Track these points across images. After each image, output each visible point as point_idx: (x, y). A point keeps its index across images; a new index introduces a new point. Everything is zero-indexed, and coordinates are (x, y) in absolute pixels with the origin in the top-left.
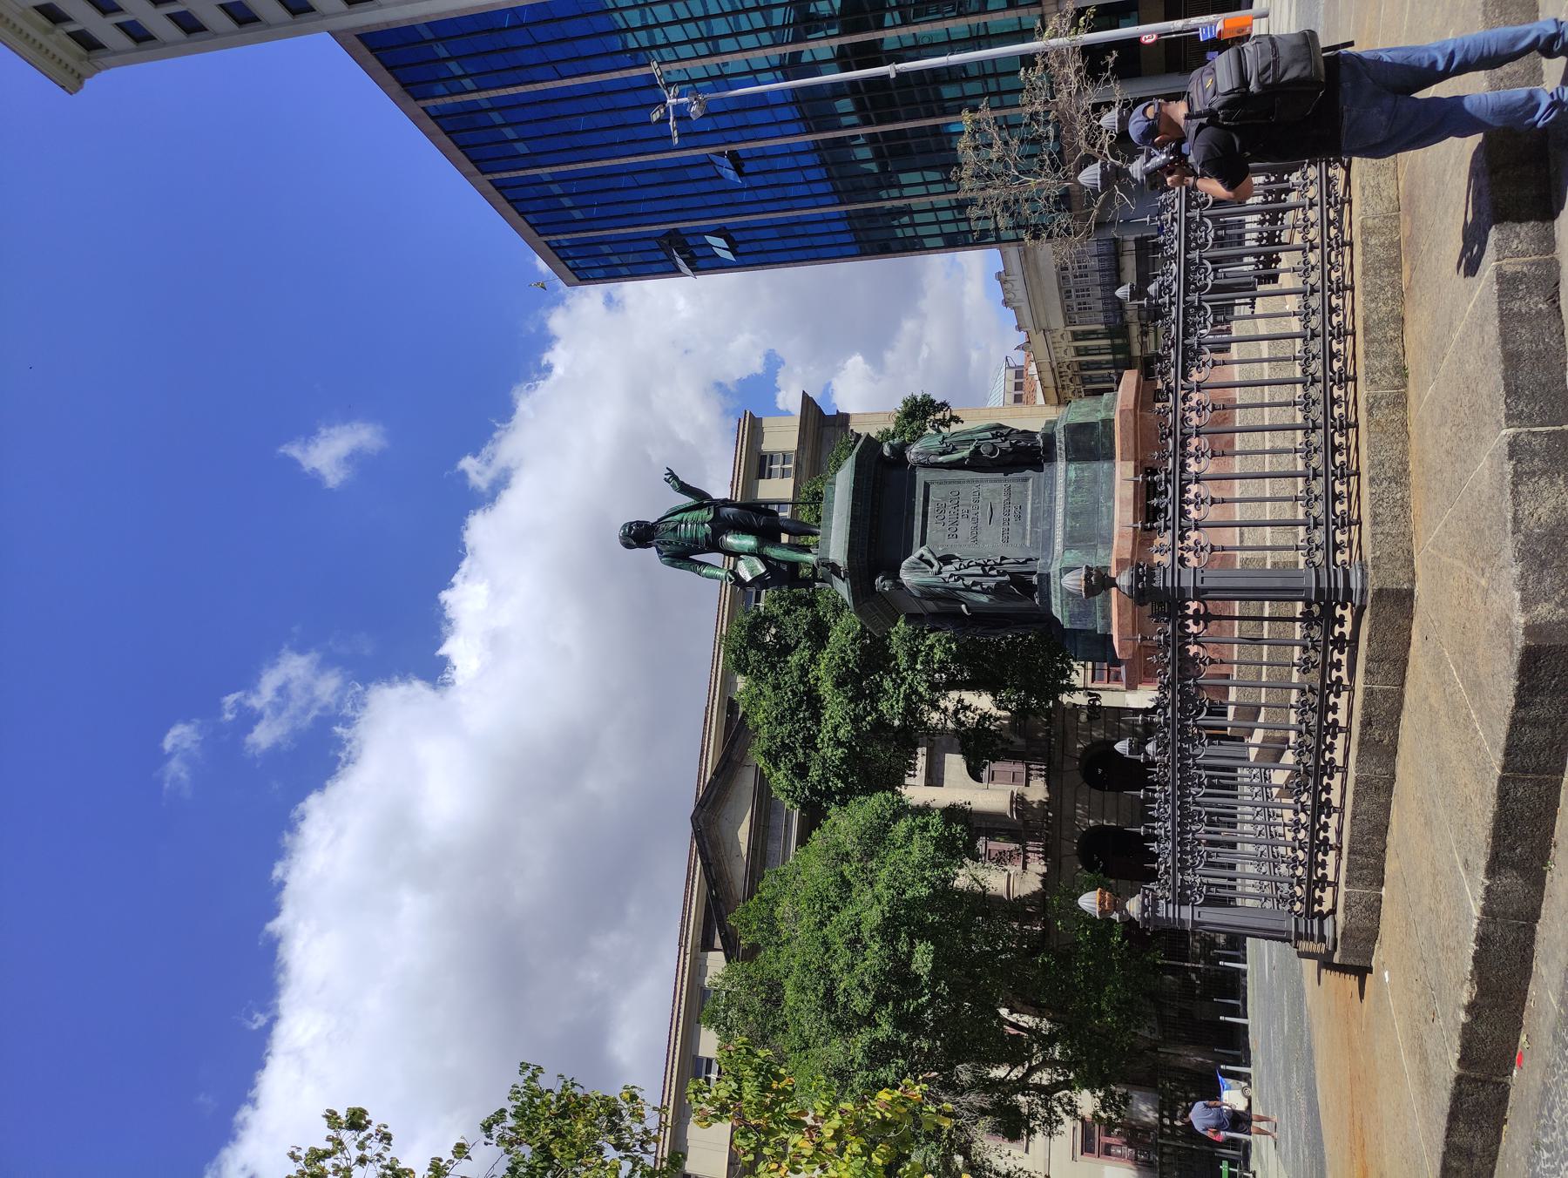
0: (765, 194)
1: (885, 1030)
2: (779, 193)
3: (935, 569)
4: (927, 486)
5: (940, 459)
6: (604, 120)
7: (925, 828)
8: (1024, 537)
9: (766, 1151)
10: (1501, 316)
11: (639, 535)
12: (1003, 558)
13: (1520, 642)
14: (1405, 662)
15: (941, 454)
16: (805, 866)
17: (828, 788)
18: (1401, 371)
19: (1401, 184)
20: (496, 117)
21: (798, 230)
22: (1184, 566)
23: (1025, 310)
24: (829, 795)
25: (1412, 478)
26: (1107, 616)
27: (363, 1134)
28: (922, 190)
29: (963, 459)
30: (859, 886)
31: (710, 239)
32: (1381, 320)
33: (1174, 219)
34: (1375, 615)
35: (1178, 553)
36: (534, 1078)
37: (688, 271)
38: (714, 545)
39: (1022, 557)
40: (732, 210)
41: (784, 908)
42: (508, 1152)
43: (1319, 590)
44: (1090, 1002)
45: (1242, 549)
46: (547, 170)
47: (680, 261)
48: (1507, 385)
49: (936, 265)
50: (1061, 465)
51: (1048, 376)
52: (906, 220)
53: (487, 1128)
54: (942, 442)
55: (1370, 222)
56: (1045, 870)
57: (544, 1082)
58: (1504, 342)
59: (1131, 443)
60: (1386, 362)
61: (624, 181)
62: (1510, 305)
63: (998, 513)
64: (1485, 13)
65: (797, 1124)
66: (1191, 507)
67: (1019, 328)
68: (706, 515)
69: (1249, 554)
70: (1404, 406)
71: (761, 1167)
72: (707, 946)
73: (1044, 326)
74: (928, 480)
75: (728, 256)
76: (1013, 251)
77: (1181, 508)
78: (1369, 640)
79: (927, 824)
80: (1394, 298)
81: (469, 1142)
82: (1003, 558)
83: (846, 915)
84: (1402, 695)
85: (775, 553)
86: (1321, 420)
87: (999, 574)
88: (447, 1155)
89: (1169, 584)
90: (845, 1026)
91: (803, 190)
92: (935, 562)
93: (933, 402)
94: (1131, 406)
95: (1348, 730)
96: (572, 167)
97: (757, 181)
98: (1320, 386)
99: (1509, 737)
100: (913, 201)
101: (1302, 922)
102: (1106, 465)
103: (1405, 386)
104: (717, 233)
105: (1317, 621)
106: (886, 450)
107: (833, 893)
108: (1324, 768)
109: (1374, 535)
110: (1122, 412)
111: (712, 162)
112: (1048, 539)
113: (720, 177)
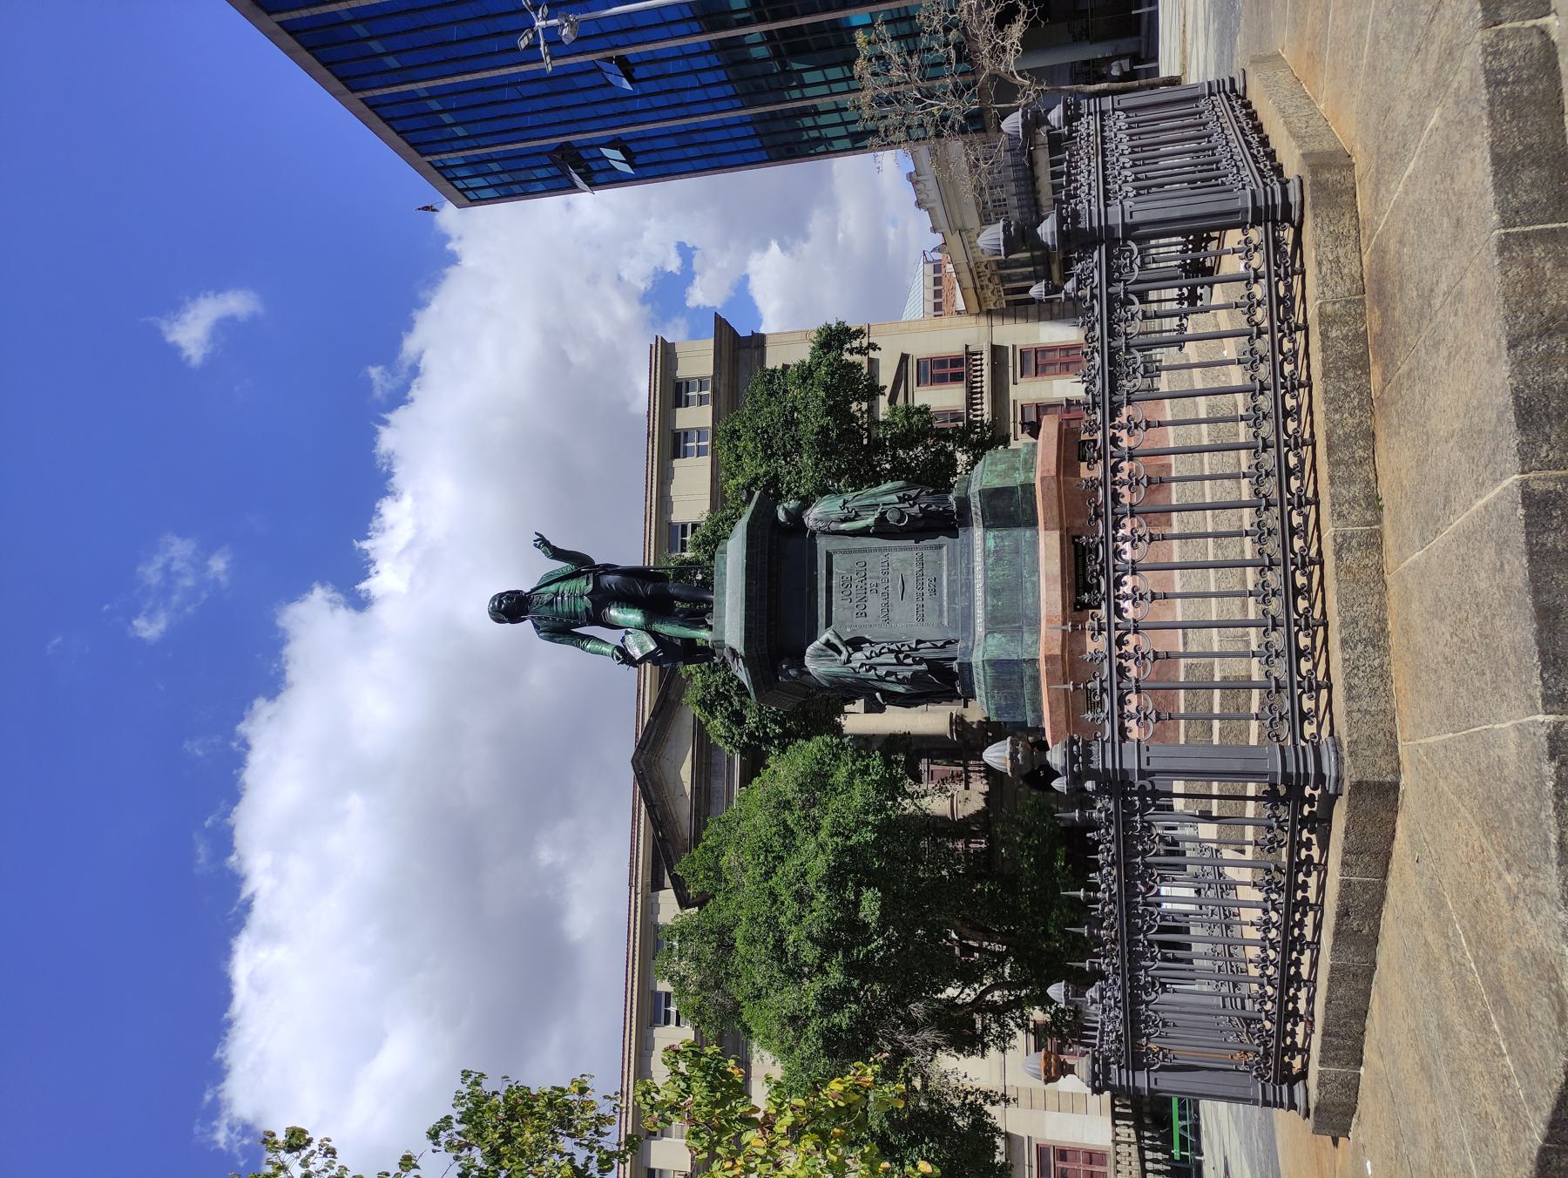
0: (658, 101)
1: (836, 977)
2: (674, 98)
3: (844, 657)
4: (829, 556)
5: (843, 526)
6: (480, 28)
7: (865, 771)
8: (941, 614)
9: (719, 1150)
11: (510, 608)
12: (919, 642)
14: (1388, 855)
17: (765, 733)
18: (1374, 502)
19: (1365, 259)
20: (360, 30)
21: (698, 138)
22: (1116, 446)
23: (940, 211)
24: (768, 740)
25: (1393, 641)
26: (1037, 710)
27: (304, 1153)
28: (824, 90)
29: (868, 527)
30: (802, 834)
31: (606, 152)
32: (1348, 436)
35: (1110, 432)
37: (585, 187)
38: (597, 618)
40: (626, 119)
41: (729, 858)
42: (457, 1158)
43: (1286, 777)
44: (1037, 927)
45: (1186, 655)
46: (422, 85)
47: (576, 177)
48: (1542, 653)
49: (845, 168)
50: (978, 532)
51: (966, 277)
52: (808, 122)
53: (434, 1135)
55: (1329, 308)
56: (987, 788)
57: (487, 1087)
58: (1536, 592)
59: (1056, 512)
60: (1356, 489)
61: (507, 93)
62: (1542, 538)
64: (1491, 115)
65: (747, 1121)
66: (1130, 663)
67: (934, 230)
68: (584, 585)
70: (1379, 547)
71: (716, 1166)
72: (657, 885)
73: (959, 225)
74: (830, 549)
75: (626, 168)
76: (923, 150)
77: (1122, 726)
79: (867, 766)
80: (1361, 407)
81: (415, 1153)
82: (919, 642)
83: (792, 863)
84: (1384, 887)
85: (667, 629)
86: (1279, 556)
87: (916, 662)
89: (1124, 1082)
90: (795, 975)
91: (699, 95)
93: (848, 329)
94: (1053, 473)
96: (449, 81)
97: (650, 87)
98: (1276, 511)
99: (1555, 1112)
100: (817, 101)
101: (1270, 1088)
102: (1028, 533)
103: (1379, 521)
104: (614, 144)
105: (1284, 801)
106: (782, 516)
107: (777, 843)
108: (1293, 942)
109: (1349, 713)
110: (1042, 479)
111: (599, 69)
113: (609, 84)
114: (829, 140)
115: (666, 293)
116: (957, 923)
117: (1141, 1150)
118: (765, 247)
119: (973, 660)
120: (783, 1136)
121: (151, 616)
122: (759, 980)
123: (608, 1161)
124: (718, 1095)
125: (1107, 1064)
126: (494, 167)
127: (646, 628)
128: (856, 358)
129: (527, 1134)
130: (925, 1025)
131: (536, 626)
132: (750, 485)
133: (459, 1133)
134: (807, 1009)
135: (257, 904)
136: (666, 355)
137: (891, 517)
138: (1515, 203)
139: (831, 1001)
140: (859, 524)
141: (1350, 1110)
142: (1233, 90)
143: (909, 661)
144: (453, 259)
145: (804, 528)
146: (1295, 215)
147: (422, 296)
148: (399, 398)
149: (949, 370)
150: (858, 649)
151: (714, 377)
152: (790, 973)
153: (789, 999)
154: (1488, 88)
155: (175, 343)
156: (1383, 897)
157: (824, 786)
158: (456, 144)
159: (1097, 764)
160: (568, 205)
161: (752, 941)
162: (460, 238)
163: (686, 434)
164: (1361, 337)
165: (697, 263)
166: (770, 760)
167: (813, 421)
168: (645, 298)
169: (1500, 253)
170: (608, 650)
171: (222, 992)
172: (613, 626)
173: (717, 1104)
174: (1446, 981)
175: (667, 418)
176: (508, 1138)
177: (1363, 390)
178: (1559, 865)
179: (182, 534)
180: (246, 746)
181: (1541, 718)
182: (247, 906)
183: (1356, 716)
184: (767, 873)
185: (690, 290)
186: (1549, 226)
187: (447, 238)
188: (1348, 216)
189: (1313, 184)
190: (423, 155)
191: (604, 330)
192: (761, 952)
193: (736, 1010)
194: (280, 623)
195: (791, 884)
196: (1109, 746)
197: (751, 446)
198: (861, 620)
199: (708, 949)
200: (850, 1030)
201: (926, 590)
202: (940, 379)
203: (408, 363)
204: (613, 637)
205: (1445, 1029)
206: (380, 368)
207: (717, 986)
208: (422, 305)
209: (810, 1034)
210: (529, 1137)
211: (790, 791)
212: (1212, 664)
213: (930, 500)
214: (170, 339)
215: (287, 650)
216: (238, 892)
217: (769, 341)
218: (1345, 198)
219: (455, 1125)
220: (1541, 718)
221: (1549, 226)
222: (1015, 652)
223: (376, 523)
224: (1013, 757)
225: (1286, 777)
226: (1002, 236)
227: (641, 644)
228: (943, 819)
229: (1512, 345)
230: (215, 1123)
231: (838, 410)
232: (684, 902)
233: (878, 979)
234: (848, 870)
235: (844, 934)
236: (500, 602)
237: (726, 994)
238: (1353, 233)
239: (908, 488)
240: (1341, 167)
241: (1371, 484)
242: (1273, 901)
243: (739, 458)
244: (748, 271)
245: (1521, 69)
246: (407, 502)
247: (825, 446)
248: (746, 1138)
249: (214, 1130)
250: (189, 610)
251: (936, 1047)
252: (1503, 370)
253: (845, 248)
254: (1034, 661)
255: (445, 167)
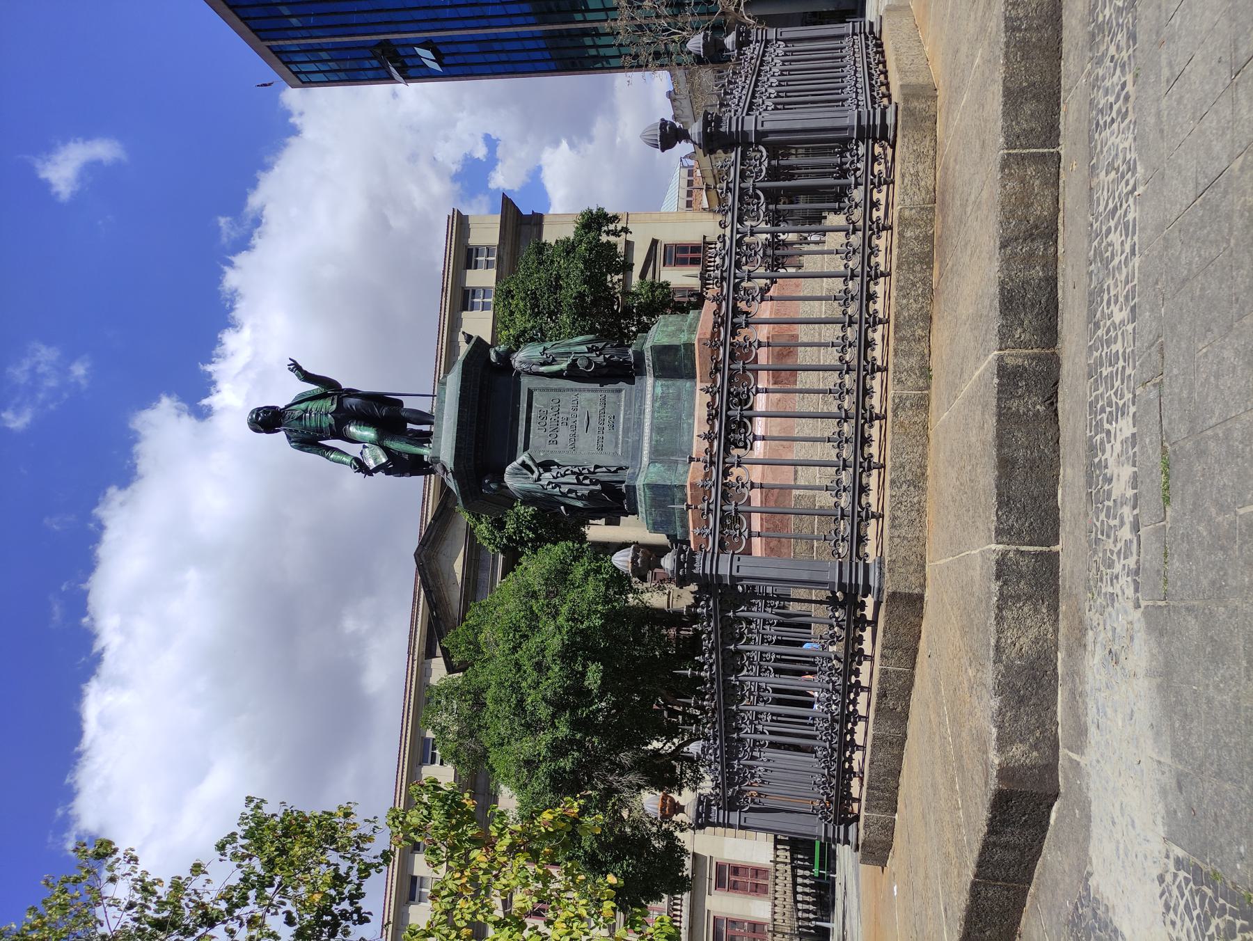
1: (563, 731)
4: (530, 393)
5: (542, 369)
7: (598, 571)
8: (616, 446)
10: (999, 415)
12: (596, 467)
13: (993, 784)
14: (916, 651)
15: (543, 364)
16: (505, 594)
17: (521, 538)
21: (497, 46)
24: (523, 543)
29: (562, 371)
30: (544, 618)
31: (420, 51)
33: (728, 189)
34: (889, 613)
36: (258, 807)
39: (613, 463)
42: (239, 866)
47: (393, 69)
48: (999, 495)
50: (650, 380)
52: (588, 41)
53: (221, 847)
54: (543, 353)
55: (907, 213)
57: (267, 810)
58: (1000, 446)
60: (914, 361)
63: (594, 421)
64: (1006, 56)
68: (329, 405)
69: (801, 492)
70: (927, 409)
72: (430, 654)
74: (532, 387)
75: (435, 66)
78: (885, 632)
81: (204, 861)
82: (596, 467)
84: (913, 676)
85: (396, 446)
87: (592, 483)
88: (185, 874)
90: (532, 727)
92: (535, 469)
93: (606, 215)
95: (869, 689)
98: (854, 375)
99: (981, 855)
101: (830, 827)
102: (688, 384)
103: (928, 388)
104: (426, 44)
105: (842, 605)
106: (493, 357)
109: (891, 538)
110: (699, 340)
112: (637, 448)
114: (607, 58)
115: (472, 175)
116: (664, 692)
117: (794, 869)
118: (557, 143)
119: (637, 483)
120: (504, 853)
121: (18, 412)
122: (502, 730)
123: (366, 870)
124: (454, 821)
125: (709, 806)
126: (324, 55)
127: (379, 443)
128: (612, 239)
129: (297, 848)
130: (631, 769)
131: (288, 438)
132: (519, 336)
133: (242, 846)
134: (539, 754)
135: (107, 656)
136: (460, 224)
137: (581, 364)
138: (1017, 129)
139: (558, 749)
140: (555, 368)
141: (888, 846)
142: (871, 32)
143: (587, 482)
144: (295, 131)
145: (511, 368)
146: (891, 135)
147: (267, 160)
148: (244, 244)
149: (690, 255)
150: (547, 470)
151: (499, 246)
152: (528, 726)
153: (526, 747)
154: (1006, 32)
155: (47, 179)
156: (912, 684)
157: (566, 580)
158: (290, 33)
159: (698, 570)
160: (395, 95)
161: (498, 701)
162: (301, 114)
163: (474, 291)
164: (929, 239)
165: (500, 152)
166: (523, 559)
167: (574, 286)
168: (456, 178)
169: (1002, 169)
170: (348, 460)
171: (71, 729)
172: (352, 441)
173: (454, 828)
174: (937, 752)
175: (458, 278)
176: (283, 851)
177: (926, 281)
178: (995, 662)
179: (49, 343)
180: (101, 527)
181: (993, 546)
182: (98, 659)
183: (897, 541)
184: (514, 648)
185: (493, 174)
186: (1041, 150)
187: (289, 114)
188: (928, 139)
189: (904, 109)
190: (263, 40)
191: (419, 200)
192: (505, 709)
193: (485, 756)
194: (131, 426)
195: (532, 657)
196: (709, 556)
197: (521, 304)
198: (552, 447)
199: (465, 705)
200: (572, 772)
201: (606, 426)
202: (681, 262)
203: (251, 216)
204: (354, 450)
205: (934, 786)
206: (229, 219)
207: (472, 734)
208: (267, 168)
209: (540, 774)
210: (297, 850)
211: (538, 585)
212: (814, 497)
213: (613, 351)
214: (43, 175)
215: (137, 448)
216: (90, 647)
217: (546, 220)
218: (928, 124)
219: (239, 840)
220: (993, 546)
221: (1041, 150)
222: (671, 479)
223: (218, 350)
224: (634, 561)
225: (842, 586)
226: (658, 132)
227: (375, 457)
228: (661, 611)
229: (1003, 246)
230: (66, 835)
231: (595, 281)
232: (451, 669)
233: (597, 733)
234: (579, 647)
235: (572, 698)
236: (258, 415)
237: (478, 742)
238: (932, 153)
239: (597, 340)
240: (927, 98)
241: (925, 357)
242: (834, 683)
243: (512, 313)
244: (542, 163)
245: (1033, 18)
246: (246, 333)
247: (582, 310)
248: (472, 855)
249: (64, 840)
250: (52, 407)
251: (640, 787)
252: (996, 265)
253: (601, 151)
254: (683, 487)
255: (281, 52)
